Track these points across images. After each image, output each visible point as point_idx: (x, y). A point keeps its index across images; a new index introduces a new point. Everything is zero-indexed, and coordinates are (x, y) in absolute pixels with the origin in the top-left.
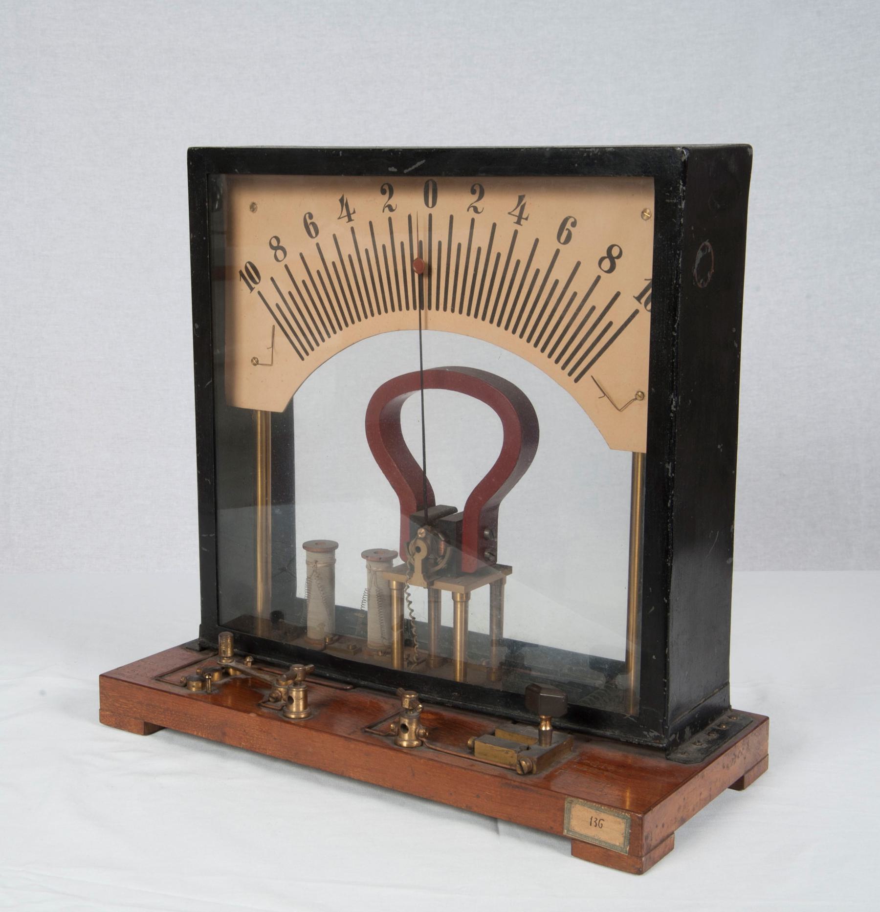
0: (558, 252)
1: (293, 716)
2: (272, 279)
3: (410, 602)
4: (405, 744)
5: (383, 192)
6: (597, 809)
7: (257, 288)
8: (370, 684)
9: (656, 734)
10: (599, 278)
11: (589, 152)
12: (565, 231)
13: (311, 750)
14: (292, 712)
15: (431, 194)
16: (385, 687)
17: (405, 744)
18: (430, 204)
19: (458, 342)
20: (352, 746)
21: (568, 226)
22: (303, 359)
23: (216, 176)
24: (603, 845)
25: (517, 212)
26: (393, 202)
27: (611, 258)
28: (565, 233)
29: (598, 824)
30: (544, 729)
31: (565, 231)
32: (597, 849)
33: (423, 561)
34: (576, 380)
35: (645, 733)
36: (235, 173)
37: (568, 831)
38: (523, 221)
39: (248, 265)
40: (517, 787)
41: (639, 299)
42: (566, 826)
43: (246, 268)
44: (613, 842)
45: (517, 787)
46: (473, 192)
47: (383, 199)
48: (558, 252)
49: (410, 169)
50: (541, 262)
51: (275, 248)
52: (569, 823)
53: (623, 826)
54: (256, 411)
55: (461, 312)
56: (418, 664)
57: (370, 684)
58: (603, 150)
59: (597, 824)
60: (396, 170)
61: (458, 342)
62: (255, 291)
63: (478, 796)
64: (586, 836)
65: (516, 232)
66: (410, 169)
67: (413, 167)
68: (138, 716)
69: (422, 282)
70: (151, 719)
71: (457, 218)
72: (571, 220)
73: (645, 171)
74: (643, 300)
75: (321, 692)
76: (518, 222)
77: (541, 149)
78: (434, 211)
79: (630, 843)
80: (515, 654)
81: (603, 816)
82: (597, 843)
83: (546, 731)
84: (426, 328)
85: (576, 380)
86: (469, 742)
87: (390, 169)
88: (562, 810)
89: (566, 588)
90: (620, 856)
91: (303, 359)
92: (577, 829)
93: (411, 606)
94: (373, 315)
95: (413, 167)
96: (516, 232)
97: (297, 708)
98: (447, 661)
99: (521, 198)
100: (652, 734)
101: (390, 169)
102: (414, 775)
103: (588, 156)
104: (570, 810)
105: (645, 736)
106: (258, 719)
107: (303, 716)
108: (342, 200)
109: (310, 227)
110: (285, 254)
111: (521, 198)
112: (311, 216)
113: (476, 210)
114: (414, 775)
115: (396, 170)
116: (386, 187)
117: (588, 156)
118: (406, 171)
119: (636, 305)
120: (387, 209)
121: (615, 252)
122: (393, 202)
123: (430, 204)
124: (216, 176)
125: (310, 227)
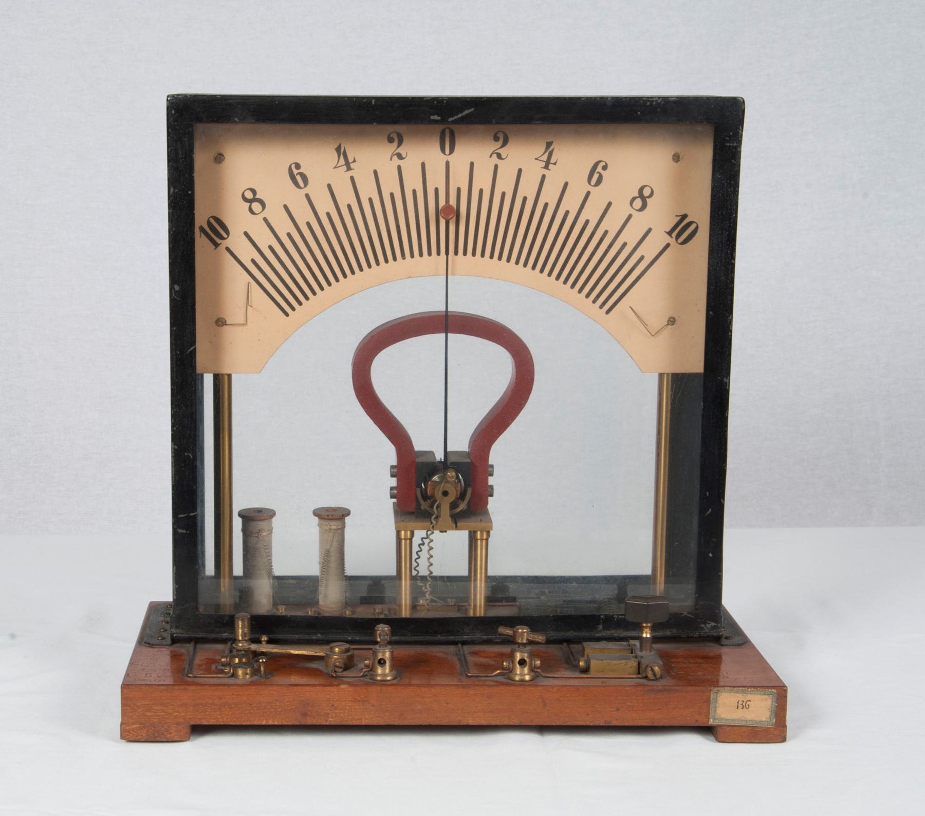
0: (307, 196)
1: (379, 678)
2: (246, 234)
3: (431, 548)
4: (517, 678)
5: (391, 140)
6: (744, 692)
7: (225, 243)
8: (403, 638)
9: (713, 624)
10: (630, 216)
11: (652, 102)
12: (595, 175)
13: (420, 707)
14: (377, 675)
15: (448, 141)
16: (421, 638)
17: (517, 678)
18: (447, 151)
19: (412, 287)
20: (472, 692)
21: (599, 169)
22: (287, 315)
23: (716, 124)
24: (750, 724)
25: (545, 158)
26: (502, 152)
27: (643, 198)
28: (596, 176)
29: (745, 706)
30: (644, 635)
31: (595, 175)
32: (744, 729)
33: (451, 504)
34: (608, 312)
35: (703, 626)
36: (235, 122)
37: (714, 719)
38: (551, 166)
39: (212, 220)
40: (661, 691)
41: (670, 233)
42: (711, 716)
43: (209, 224)
44: (759, 719)
45: (661, 691)
46: (496, 139)
47: (392, 148)
48: (307, 196)
49: (456, 117)
50: (571, 204)
51: (250, 201)
52: (715, 711)
53: (770, 701)
54: (222, 375)
55: (412, 256)
56: (428, 610)
57: (403, 638)
58: (666, 100)
59: (745, 706)
60: (439, 118)
61: (412, 287)
62: (222, 248)
63: (618, 710)
64: (733, 720)
65: (544, 177)
66: (456, 117)
67: (460, 116)
68: (181, 720)
69: (449, 225)
70: (200, 719)
71: (470, 164)
72: (293, 166)
73: (708, 120)
74: (674, 235)
75: (406, 651)
76: (546, 167)
77: (602, 98)
78: (452, 159)
79: (776, 716)
80: (499, 588)
81: (750, 697)
82: (744, 723)
83: (646, 638)
84: (453, 275)
85: (608, 312)
86: (581, 664)
87: (432, 117)
88: (708, 701)
89: (574, 511)
90: (766, 730)
91: (287, 315)
92: (723, 716)
93: (431, 552)
94: (386, 261)
95: (460, 116)
96: (544, 177)
97: (384, 672)
98: (464, 600)
99: (549, 144)
100: (708, 626)
101: (432, 117)
102: (545, 705)
103: (651, 104)
104: (716, 701)
105: (703, 628)
106: (351, 689)
107: (389, 678)
108: (338, 150)
109: (298, 177)
110: (263, 205)
111: (549, 144)
112: (298, 166)
113: (499, 156)
114: (545, 705)
115: (439, 118)
116: (395, 136)
117: (651, 104)
118: (450, 119)
119: (668, 239)
120: (404, 156)
121: (646, 192)
122: (502, 152)
123: (447, 151)
124: (716, 124)
125: (298, 177)
